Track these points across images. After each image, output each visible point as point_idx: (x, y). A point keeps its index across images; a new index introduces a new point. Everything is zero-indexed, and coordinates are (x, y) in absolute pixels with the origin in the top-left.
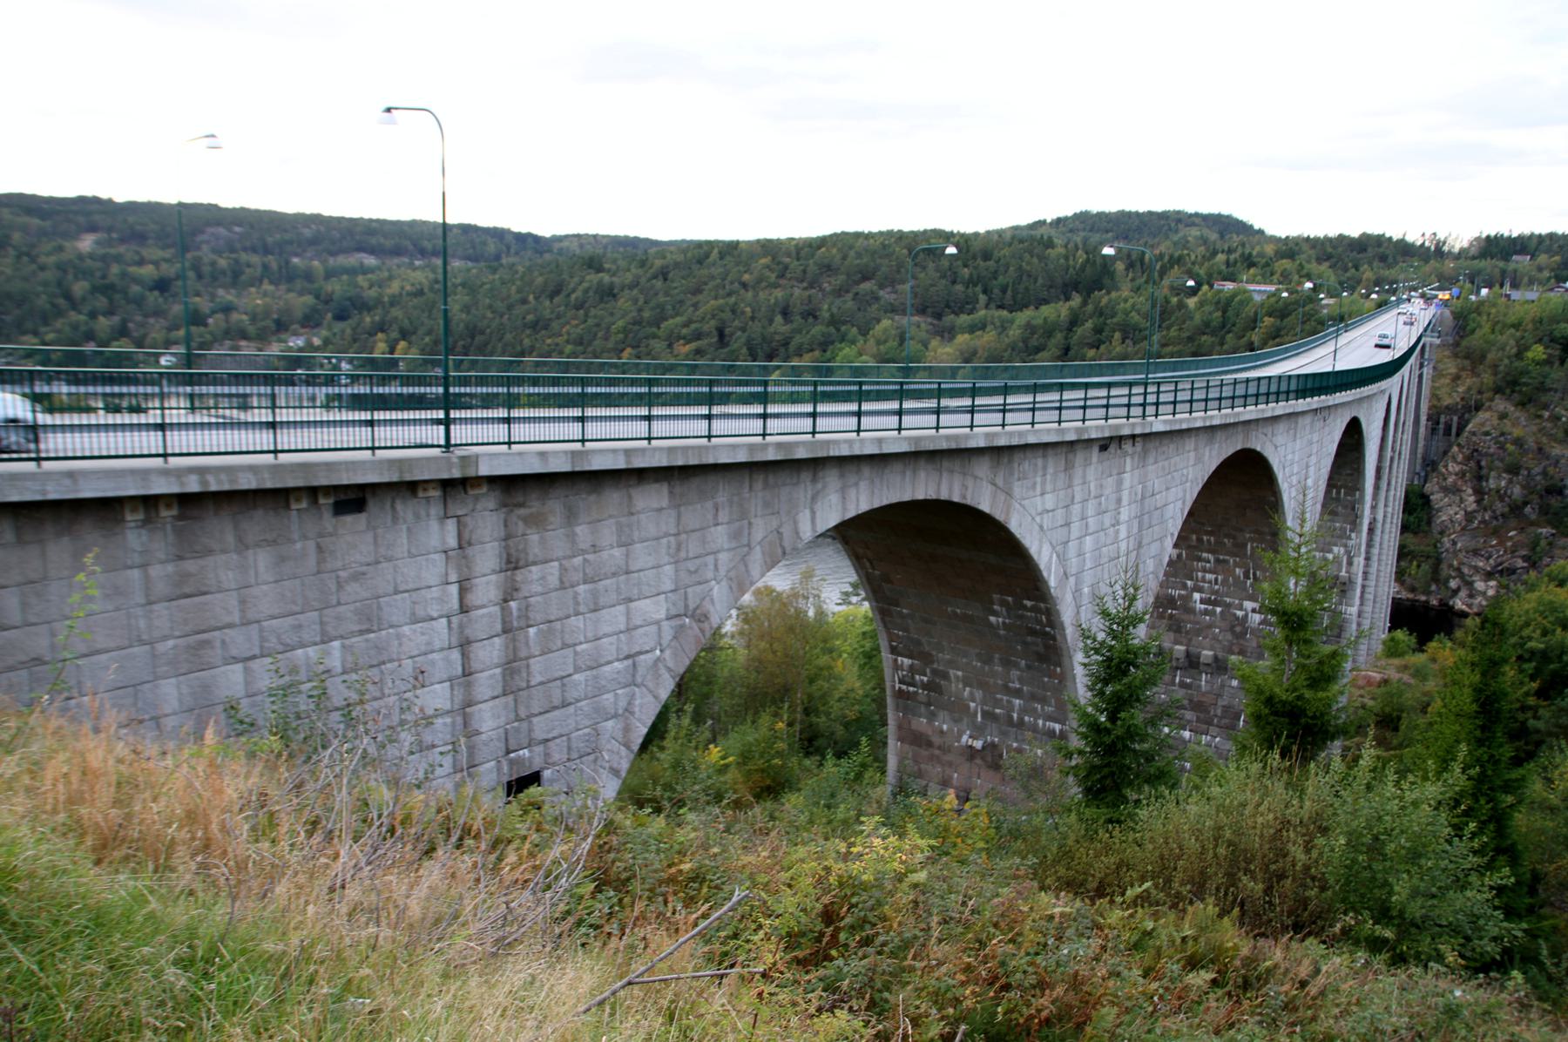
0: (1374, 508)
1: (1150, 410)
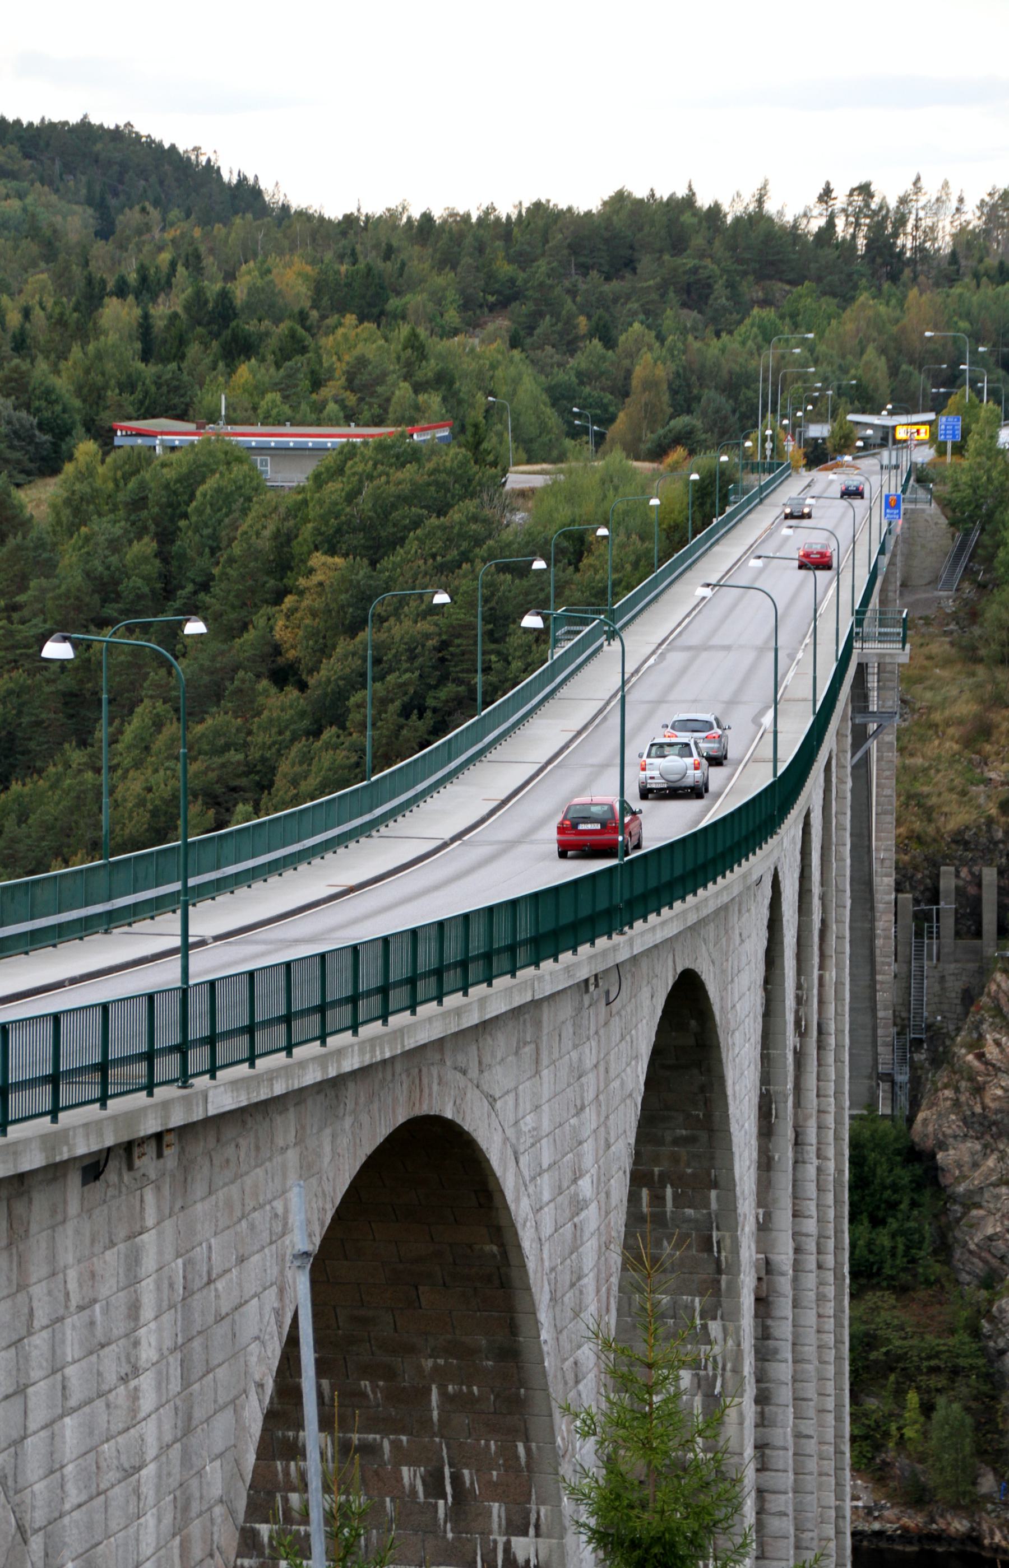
0: (764, 1227)
1: (198, 1057)
